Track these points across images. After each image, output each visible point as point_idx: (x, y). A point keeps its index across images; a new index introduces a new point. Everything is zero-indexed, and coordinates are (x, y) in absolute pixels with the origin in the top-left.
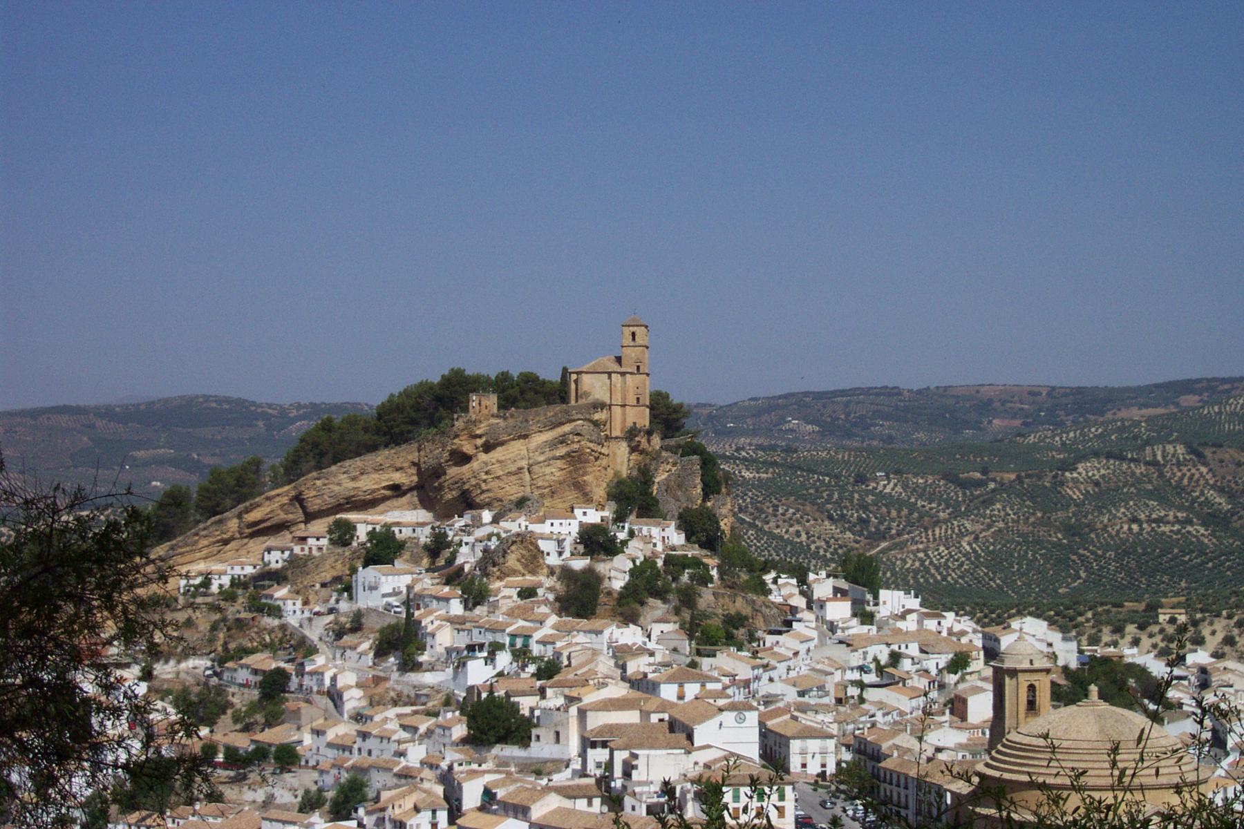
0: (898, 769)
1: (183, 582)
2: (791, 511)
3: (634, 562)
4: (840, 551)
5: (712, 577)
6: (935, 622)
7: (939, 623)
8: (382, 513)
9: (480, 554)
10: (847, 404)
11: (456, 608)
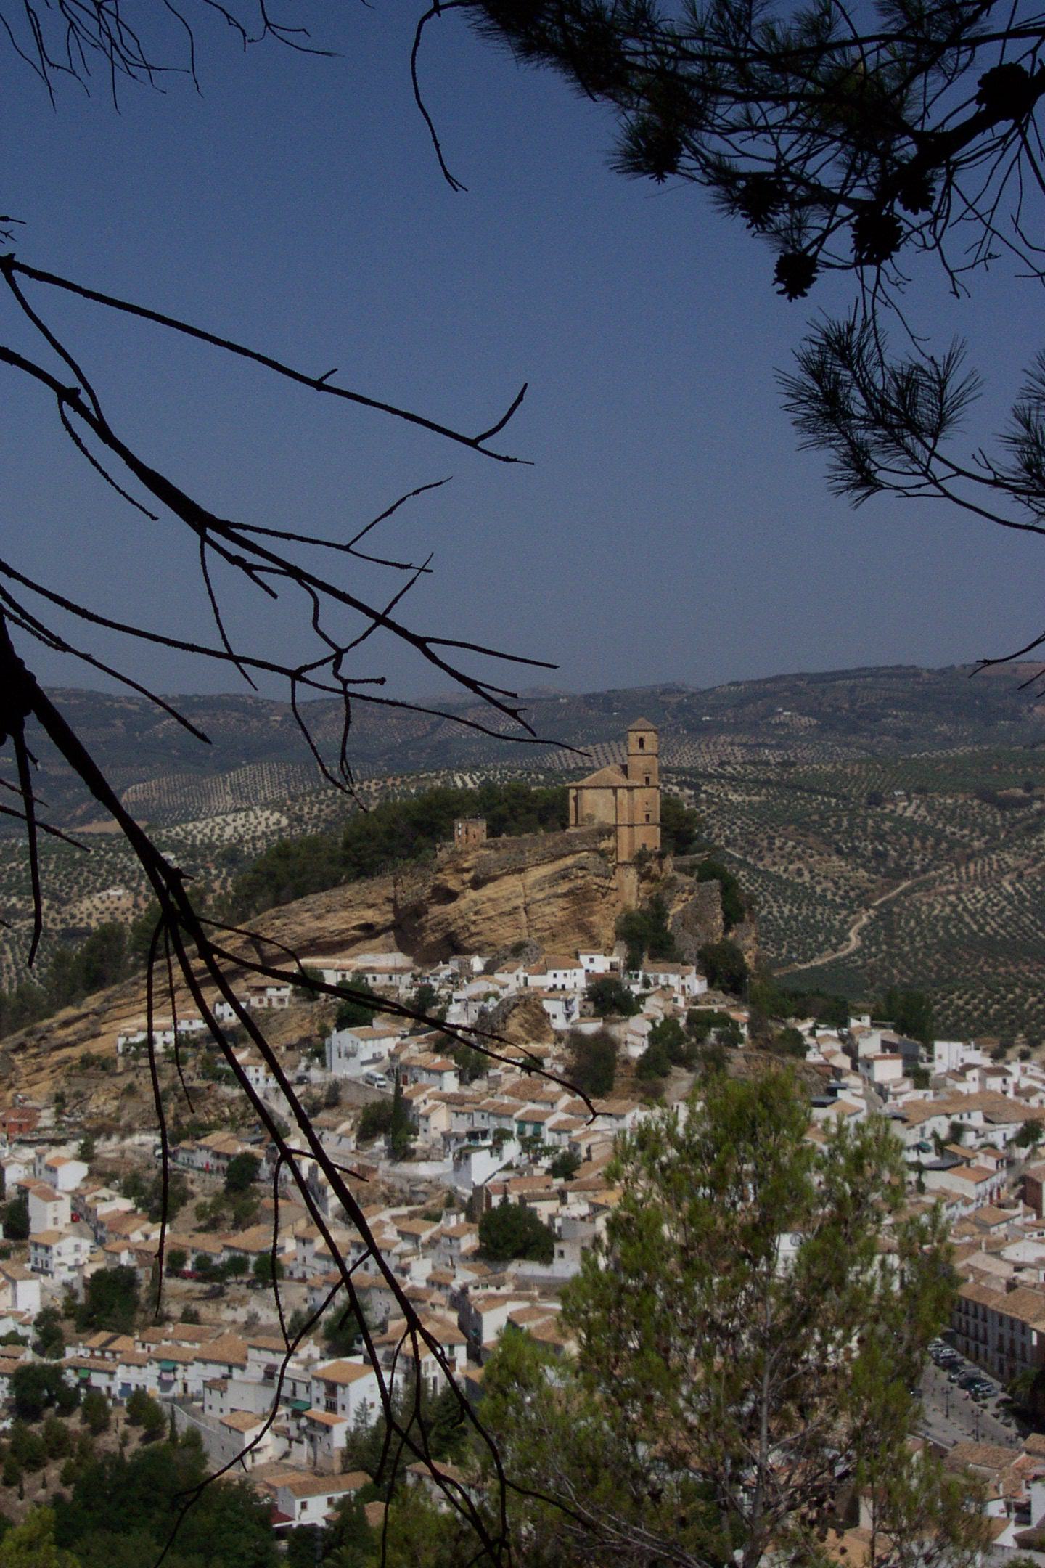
0: (975, 1298)
1: (121, 1041)
2: (791, 843)
3: (653, 1022)
4: (852, 894)
5: (742, 1036)
6: (999, 1080)
7: (1005, 1081)
8: (352, 957)
9: (475, 1016)
10: (852, 689)
11: (451, 1083)
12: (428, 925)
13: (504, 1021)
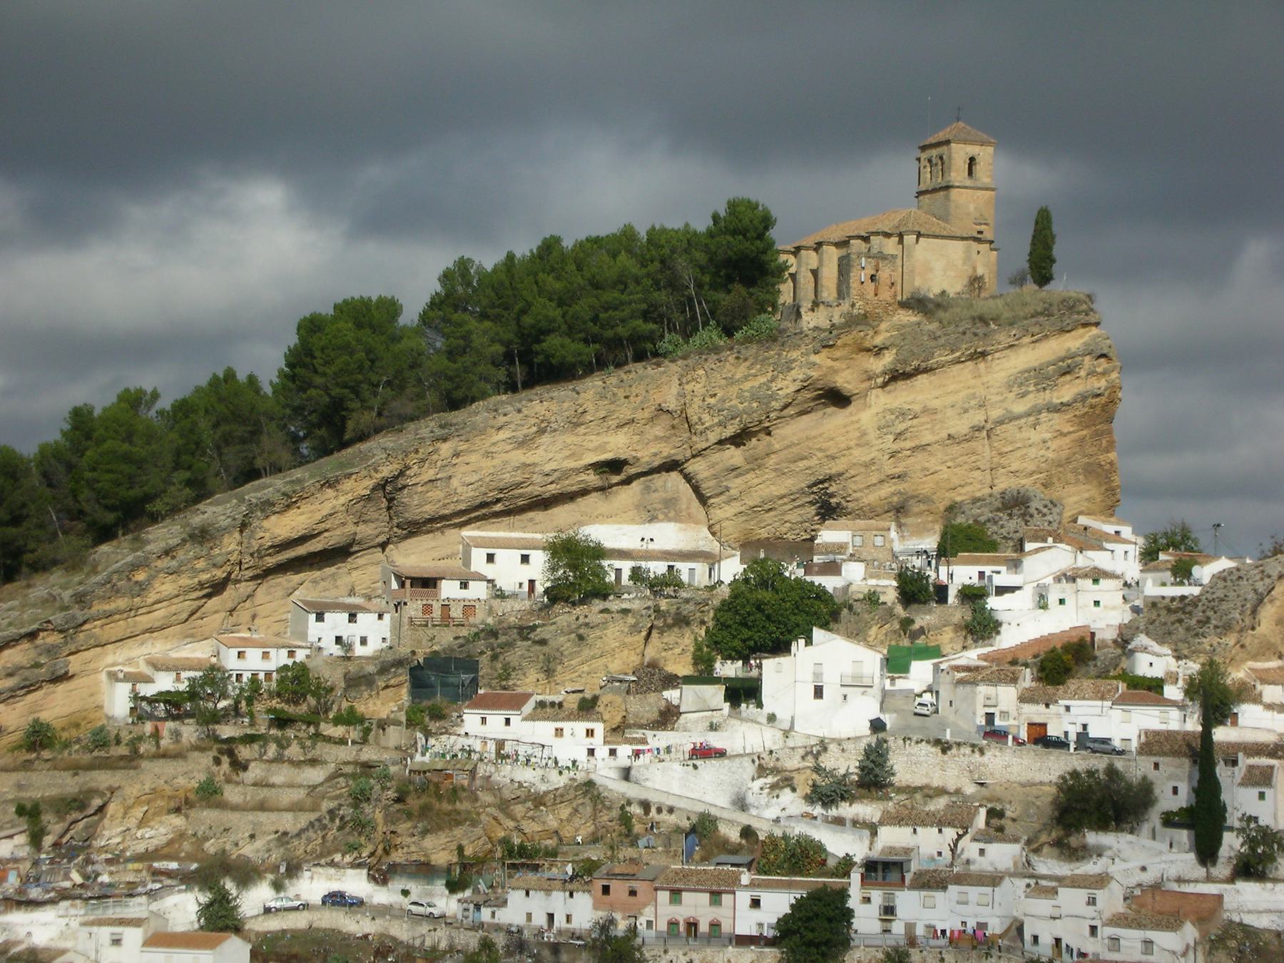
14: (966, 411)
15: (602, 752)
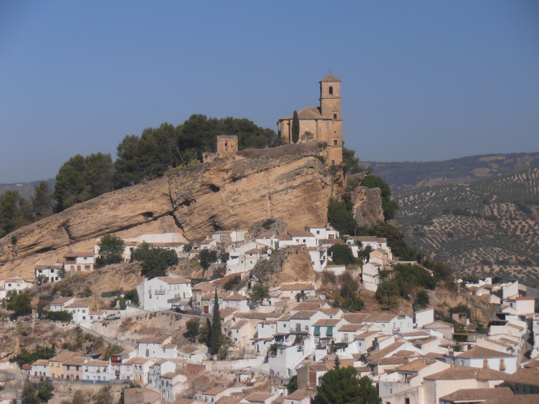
12: (197, 210)
13: (281, 265)
14: (259, 190)
15: (88, 318)
